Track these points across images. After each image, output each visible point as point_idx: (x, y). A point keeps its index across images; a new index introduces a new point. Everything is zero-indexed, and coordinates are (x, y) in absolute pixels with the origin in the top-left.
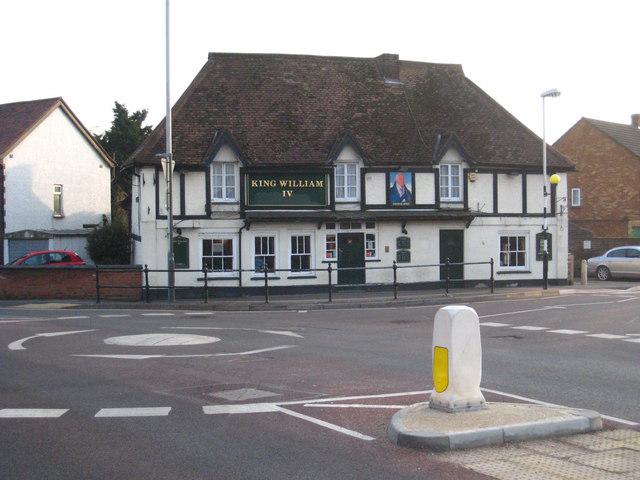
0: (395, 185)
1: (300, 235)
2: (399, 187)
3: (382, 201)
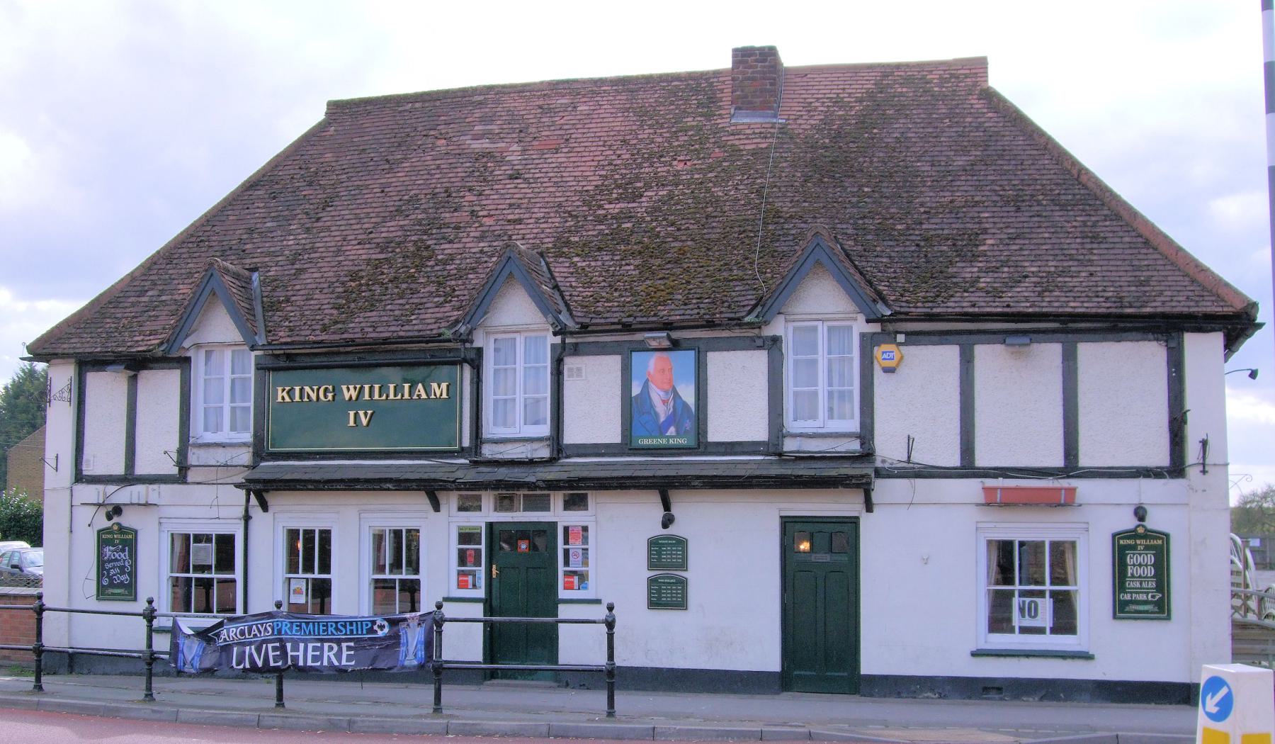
0: (646, 387)
1: (309, 526)
2: (657, 396)
3: (611, 434)
